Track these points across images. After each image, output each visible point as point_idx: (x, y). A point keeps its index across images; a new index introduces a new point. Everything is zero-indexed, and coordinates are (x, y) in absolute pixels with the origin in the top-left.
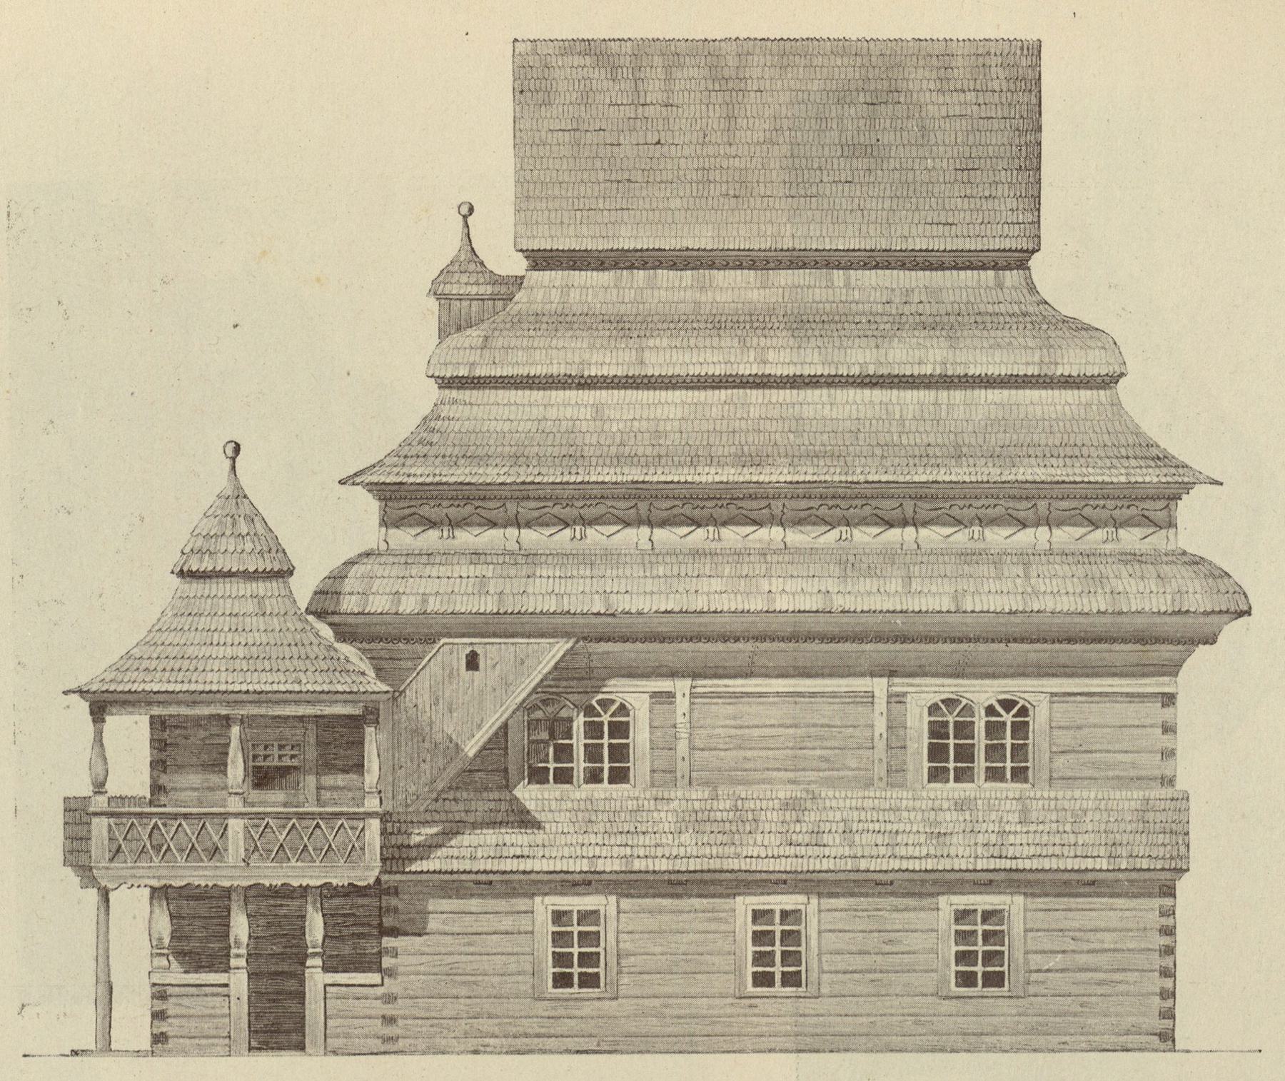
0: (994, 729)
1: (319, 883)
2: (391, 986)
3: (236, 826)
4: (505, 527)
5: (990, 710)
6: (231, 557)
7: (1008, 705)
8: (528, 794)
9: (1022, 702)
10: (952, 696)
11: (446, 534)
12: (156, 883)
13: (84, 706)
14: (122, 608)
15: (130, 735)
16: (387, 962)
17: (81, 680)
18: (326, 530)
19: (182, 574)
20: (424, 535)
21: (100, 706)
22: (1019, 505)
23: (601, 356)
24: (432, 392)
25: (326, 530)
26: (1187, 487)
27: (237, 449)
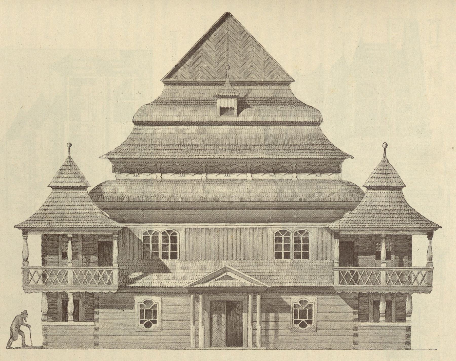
0: (297, 240)
1: (84, 291)
2: (97, 325)
3: (383, 273)
4: (292, 173)
5: (164, 233)
6: (68, 180)
7: (301, 232)
8: (168, 262)
9: (306, 231)
10: (170, 229)
11: (318, 175)
12: (74, 291)
13: (21, 231)
14: (34, 199)
15: (36, 240)
16: (96, 317)
17: (18, 222)
18: (99, 172)
19: (54, 188)
20: (311, 175)
21: (26, 232)
22: (332, 165)
23: (156, 113)
24: (133, 125)
25: (99, 172)
26: (343, 159)
27: (71, 145)
